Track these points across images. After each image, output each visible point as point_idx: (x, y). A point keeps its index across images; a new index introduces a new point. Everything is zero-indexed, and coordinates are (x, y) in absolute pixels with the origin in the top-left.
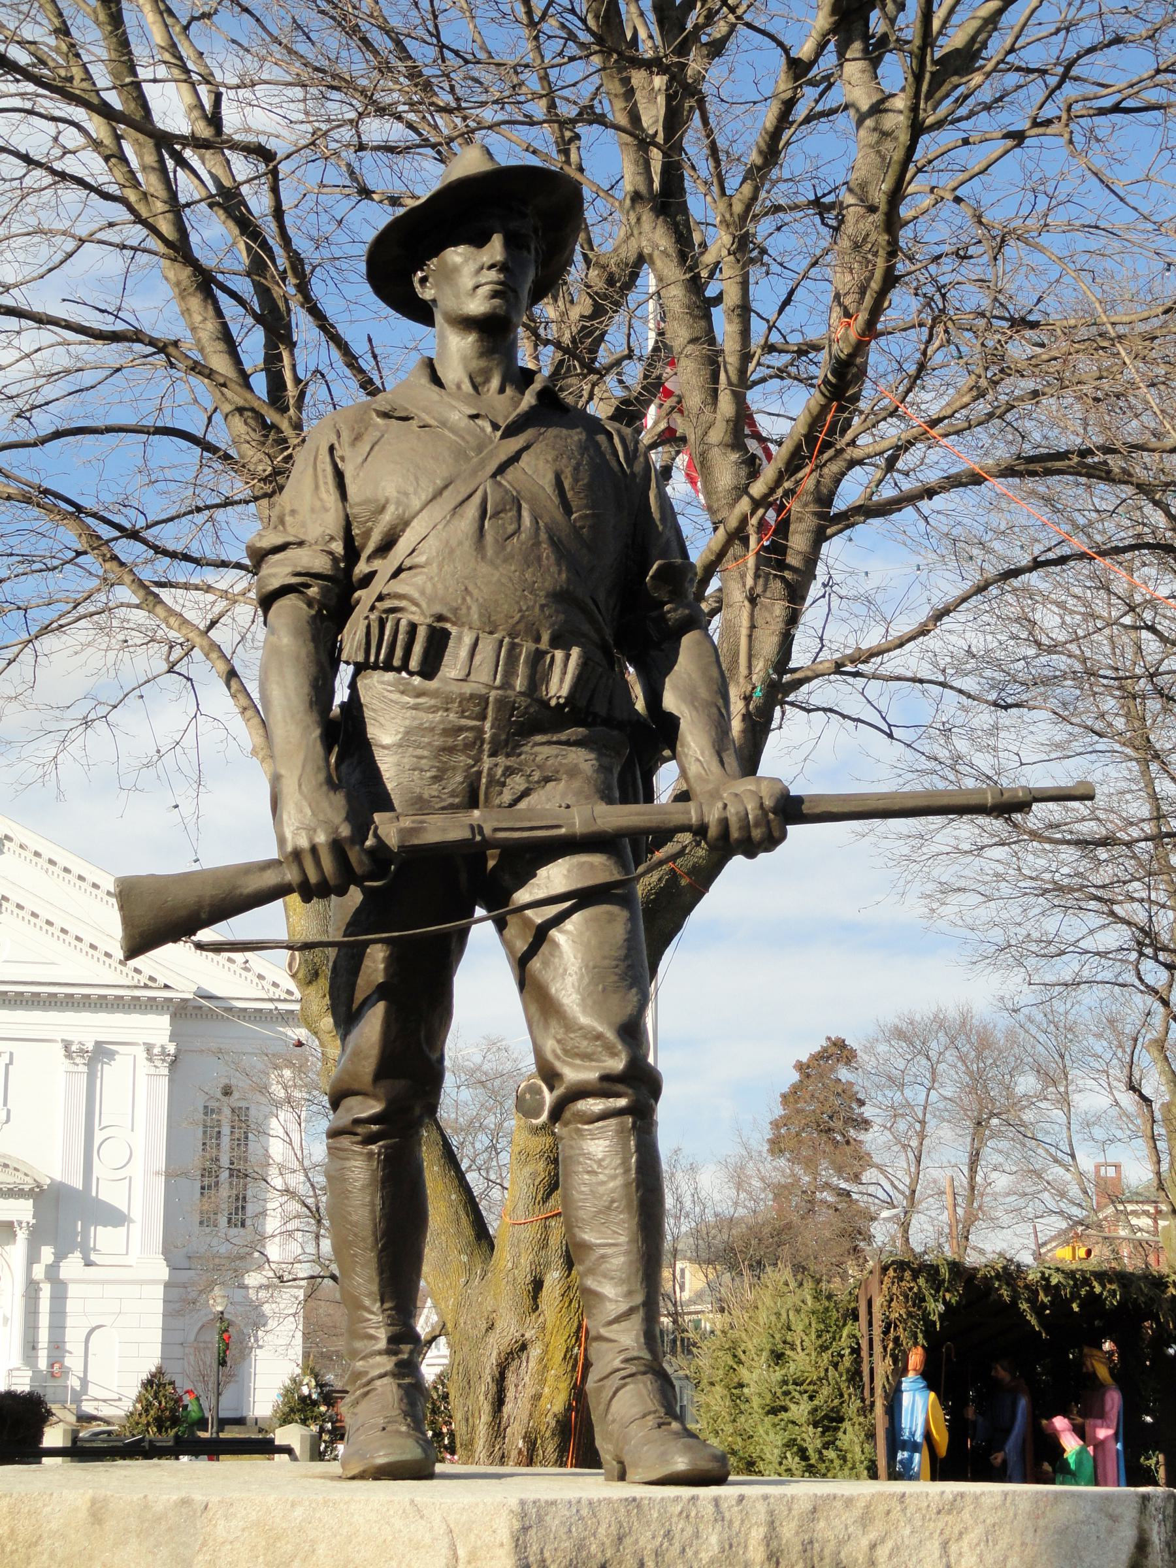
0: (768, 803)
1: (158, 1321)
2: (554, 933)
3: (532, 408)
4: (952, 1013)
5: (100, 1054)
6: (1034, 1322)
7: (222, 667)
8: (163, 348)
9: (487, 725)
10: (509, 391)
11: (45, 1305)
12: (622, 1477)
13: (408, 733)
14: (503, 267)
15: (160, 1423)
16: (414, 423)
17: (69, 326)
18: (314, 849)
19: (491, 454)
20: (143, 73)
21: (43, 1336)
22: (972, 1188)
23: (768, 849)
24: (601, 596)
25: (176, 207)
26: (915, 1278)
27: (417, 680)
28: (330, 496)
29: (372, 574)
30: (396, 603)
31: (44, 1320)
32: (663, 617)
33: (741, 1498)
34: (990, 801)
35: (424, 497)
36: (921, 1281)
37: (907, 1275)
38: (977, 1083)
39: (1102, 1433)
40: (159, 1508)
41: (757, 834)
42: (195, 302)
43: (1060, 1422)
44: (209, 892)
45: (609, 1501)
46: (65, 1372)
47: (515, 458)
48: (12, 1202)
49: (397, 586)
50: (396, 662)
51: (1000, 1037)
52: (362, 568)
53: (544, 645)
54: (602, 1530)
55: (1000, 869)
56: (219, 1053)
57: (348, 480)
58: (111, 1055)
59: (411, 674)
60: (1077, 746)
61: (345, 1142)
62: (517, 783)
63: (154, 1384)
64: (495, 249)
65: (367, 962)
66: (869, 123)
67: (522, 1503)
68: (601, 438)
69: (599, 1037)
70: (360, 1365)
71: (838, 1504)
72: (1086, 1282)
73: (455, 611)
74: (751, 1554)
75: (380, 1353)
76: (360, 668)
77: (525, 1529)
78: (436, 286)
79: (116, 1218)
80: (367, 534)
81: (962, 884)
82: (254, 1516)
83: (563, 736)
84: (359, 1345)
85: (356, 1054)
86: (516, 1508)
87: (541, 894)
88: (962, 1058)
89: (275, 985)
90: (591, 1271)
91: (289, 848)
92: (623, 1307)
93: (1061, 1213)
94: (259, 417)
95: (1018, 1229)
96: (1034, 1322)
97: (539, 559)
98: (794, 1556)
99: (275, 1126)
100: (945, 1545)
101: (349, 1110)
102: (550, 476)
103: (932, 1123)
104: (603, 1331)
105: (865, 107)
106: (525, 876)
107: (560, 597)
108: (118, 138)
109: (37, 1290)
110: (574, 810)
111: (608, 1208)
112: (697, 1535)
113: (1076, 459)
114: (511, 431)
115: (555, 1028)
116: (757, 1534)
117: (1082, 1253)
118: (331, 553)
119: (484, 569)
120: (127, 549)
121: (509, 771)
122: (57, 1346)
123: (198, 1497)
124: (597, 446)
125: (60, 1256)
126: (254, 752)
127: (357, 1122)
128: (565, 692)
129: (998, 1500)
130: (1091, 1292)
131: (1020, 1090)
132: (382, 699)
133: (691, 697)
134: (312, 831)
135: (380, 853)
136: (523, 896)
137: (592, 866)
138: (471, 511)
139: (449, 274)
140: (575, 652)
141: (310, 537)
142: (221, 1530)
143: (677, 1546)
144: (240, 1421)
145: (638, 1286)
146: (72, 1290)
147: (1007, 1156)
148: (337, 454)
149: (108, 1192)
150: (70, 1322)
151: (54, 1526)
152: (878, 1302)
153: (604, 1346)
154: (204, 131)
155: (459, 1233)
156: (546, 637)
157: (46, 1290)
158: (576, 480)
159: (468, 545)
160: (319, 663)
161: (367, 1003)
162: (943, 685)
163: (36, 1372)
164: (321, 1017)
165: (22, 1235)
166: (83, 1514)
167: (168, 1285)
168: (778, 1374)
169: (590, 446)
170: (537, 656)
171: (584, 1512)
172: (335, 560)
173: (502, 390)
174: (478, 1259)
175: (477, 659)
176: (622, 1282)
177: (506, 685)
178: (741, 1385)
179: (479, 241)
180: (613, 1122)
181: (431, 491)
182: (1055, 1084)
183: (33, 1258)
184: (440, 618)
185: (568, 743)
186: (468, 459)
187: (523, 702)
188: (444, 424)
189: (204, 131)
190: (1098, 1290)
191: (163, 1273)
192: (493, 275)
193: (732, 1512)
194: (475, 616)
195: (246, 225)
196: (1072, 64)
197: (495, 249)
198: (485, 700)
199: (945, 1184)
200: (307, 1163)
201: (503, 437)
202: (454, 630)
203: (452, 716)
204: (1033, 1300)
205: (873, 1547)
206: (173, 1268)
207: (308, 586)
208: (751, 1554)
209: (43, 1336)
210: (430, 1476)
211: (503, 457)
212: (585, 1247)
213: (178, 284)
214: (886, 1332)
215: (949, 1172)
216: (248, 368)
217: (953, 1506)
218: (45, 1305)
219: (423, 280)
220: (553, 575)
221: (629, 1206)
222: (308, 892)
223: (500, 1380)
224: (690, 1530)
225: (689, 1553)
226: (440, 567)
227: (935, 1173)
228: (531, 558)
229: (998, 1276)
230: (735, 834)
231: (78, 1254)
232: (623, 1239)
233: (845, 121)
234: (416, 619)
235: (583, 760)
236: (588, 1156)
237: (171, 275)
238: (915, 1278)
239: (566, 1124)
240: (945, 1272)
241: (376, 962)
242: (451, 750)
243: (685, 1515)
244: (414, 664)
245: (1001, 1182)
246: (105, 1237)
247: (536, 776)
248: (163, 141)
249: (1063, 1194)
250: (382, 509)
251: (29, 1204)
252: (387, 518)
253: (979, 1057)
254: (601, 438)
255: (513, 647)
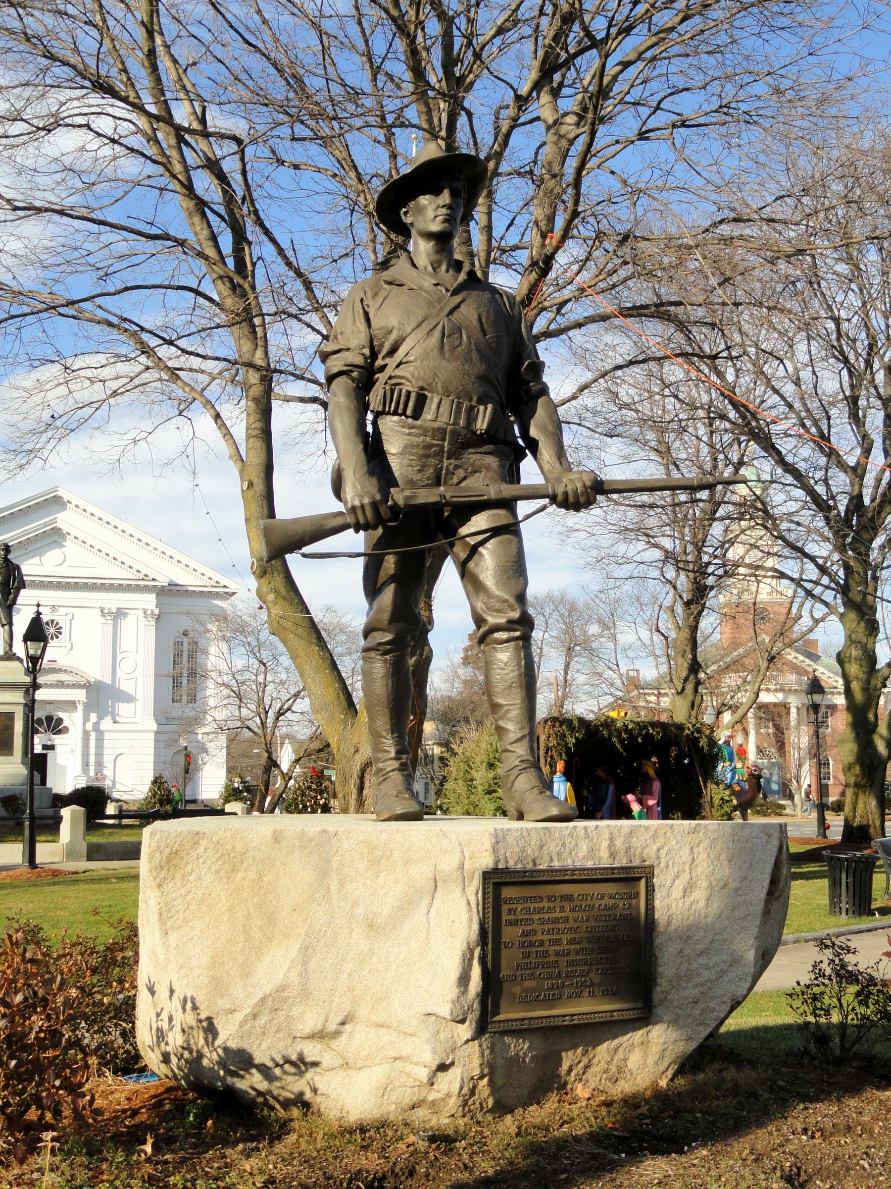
0: (588, 484)
1: (152, 751)
2: (481, 549)
3: (465, 281)
4: (557, 594)
5: (119, 614)
6: (618, 746)
7: (213, 413)
8: (182, 243)
9: (446, 444)
10: (451, 271)
11: (92, 743)
12: (521, 817)
13: (405, 447)
14: (449, 207)
15: (161, 802)
16: (405, 288)
17: (132, 231)
18: (362, 507)
19: (446, 304)
20: (169, 95)
21: (92, 759)
22: (566, 681)
23: (586, 508)
24: (500, 377)
25: (186, 169)
26: (561, 726)
27: (410, 421)
28: (362, 325)
29: (386, 365)
30: (399, 381)
31: (92, 751)
32: (529, 389)
33: (597, 827)
34: (696, 483)
35: (412, 326)
36: (564, 727)
37: (557, 724)
38: (569, 629)
39: (651, 802)
40: (311, 835)
41: (582, 499)
42: (197, 219)
43: (630, 797)
44: (308, 528)
45: (536, 829)
46: (104, 777)
47: (458, 306)
48: (74, 691)
49: (400, 372)
50: (400, 411)
51: (580, 604)
52: (379, 362)
53: (474, 403)
54: (533, 843)
55: (598, 520)
56: (188, 613)
57: (371, 316)
58: (126, 615)
59: (407, 417)
60: (636, 457)
61: (372, 654)
62: (461, 473)
63: (157, 781)
64: (445, 197)
65: (385, 564)
66: (552, 131)
67: (496, 830)
68: (497, 296)
69: (506, 601)
70: (381, 765)
71: (642, 829)
72: (645, 727)
73: (430, 385)
74: (602, 854)
75: (392, 759)
76: (378, 415)
77: (498, 842)
78: (414, 216)
79: (129, 698)
80: (382, 345)
81: (576, 527)
82: (361, 838)
83: (483, 450)
84: (380, 755)
85: (380, 610)
86: (493, 832)
87: (473, 530)
88: (562, 616)
89: (210, 578)
90: (502, 718)
91: (350, 506)
92: (519, 735)
93: (611, 694)
94: (231, 280)
95: (589, 702)
96: (618, 746)
97: (471, 359)
98: (622, 855)
99: (213, 650)
100: (692, 849)
101: (374, 638)
102: (475, 316)
103: (545, 649)
104: (509, 747)
105: (550, 122)
106: (465, 520)
107: (483, 379)
108: (154, 130)
109: (89, 736)
110: (491, 487)
111: (511, 686)
112: (577, 845)
113: (653, 308)
114: (456, 292)
115: (482, 597)
116: (605, 844)
117: (622, 714)
118: (363, 354)
119: (444, 364)
120: (164, 352)
121: (457, 467)
122: (99, 764)
123: (331, 829)
124: (496, 301)
125: (100, 718)
126: (231, 457)
127: (380, 644)
128: (484, 427)
129: (716, 827)
130: (648, 733)
131: (591, 632)
132: (391, 430)
133: (543, 429)
134: (361, 497)
135: (395, 509)
136: (464, 530)
137: (499, 516)
138: (437, 333)
139: (421, 210)
140: (490, 406)
141: (352, 346)
142: (345, 845)
143: (568, 850)
144: (194, 801)
145: (526, 725)
146: (107, 736)
147: (584, 665)
148: (365, 303)
149: (125, 685)
150: (106, 752)
151: (254, 844)
152: (543, 738)
153: (509, 754)
154: (196, 125)
155: (340, 704)
156: (475, 399)
157: (93, 736)
158: (488, 318)
159: (436, 352)
160: (359, 411)
161: (385, 584)
162: (579, 425)
163: (89, 777)
164: (268, 594)
165: (80, 708)
166: (269, 838)
167: (156, 733)
168: (492, 774)
169: (493, 301)
170: (471, 409)
171: (525, 834)
172: (366, 358)
173: (447, 271)
174: (349, 717)
175: (441, 410)
176: (518, 723)
177: (456, 423)
178: (472, 780)
179: (437, 192)
180: (512, 643)
181: (415, 323)
182: (609, 629)
183: (86, 719)
184: (422, 388)
185: (485, 453)
186: (434, 307)
187: (464, 432)
188: (421, 288)
189: (196, 125)
190: (651, 731)
191: (154, 727)
192: (444, 211)
193: (593, 834)
194: (440, 387)
195: (222, 177)
196: (660, 102)
197: (445, 197)
198: (445, 430)
199: (553, 681)
200: (234, 670)
201: (452, 295)
202: (429, 395)
203: (428, 439)
204: (619, 737)
205: (658, 850)
206: (159, 724)
207: (352, 371)
208: (602, 854)
209: (92, 759)
210: (421, 819)
211: (452, 306)
212: (499, 706)
213: (188, 209)
214: (547, 753)
215: (554, 674)
216: (224, 253)
217: (694, 831)
218: (92, 743)
219: (406, 213)
220: (479, 368)
221: (521, 686)
222: (357, 528)
223: (362, 778)
224: (573, 843)
225: (573, 853)
226: (422, 362)
227: (547, 674)
228: (467, 359)
229: (602, 725)
230: (571, 499)
231: (109, 717)
232: (518, 702)
233: (540, 126)
234: (410, 389)
235: (492, 461)
236: (500, 661)
237: (184, 204)
238: (561, 726)
239: (488, 645)
240: (576, 723)
241: (390, 563)
242: (427, 456)
243: (571, 835)
244: (409, 412)
245: (581, 678)
246: (123, 709)
247: (470, 470)
248: (179, 132)
249: (612, 685)
250: (391, 332)
251: (83, 692)
252: (393, 337)
253: (570, 615)
254: (497, 296)
255: (459, 404)
